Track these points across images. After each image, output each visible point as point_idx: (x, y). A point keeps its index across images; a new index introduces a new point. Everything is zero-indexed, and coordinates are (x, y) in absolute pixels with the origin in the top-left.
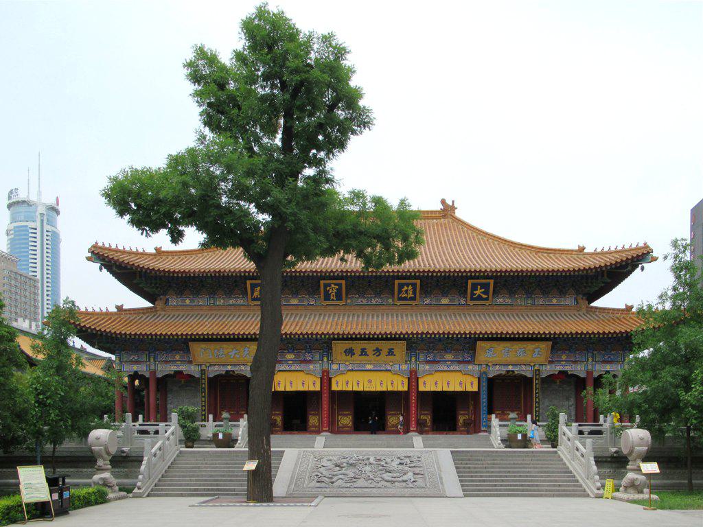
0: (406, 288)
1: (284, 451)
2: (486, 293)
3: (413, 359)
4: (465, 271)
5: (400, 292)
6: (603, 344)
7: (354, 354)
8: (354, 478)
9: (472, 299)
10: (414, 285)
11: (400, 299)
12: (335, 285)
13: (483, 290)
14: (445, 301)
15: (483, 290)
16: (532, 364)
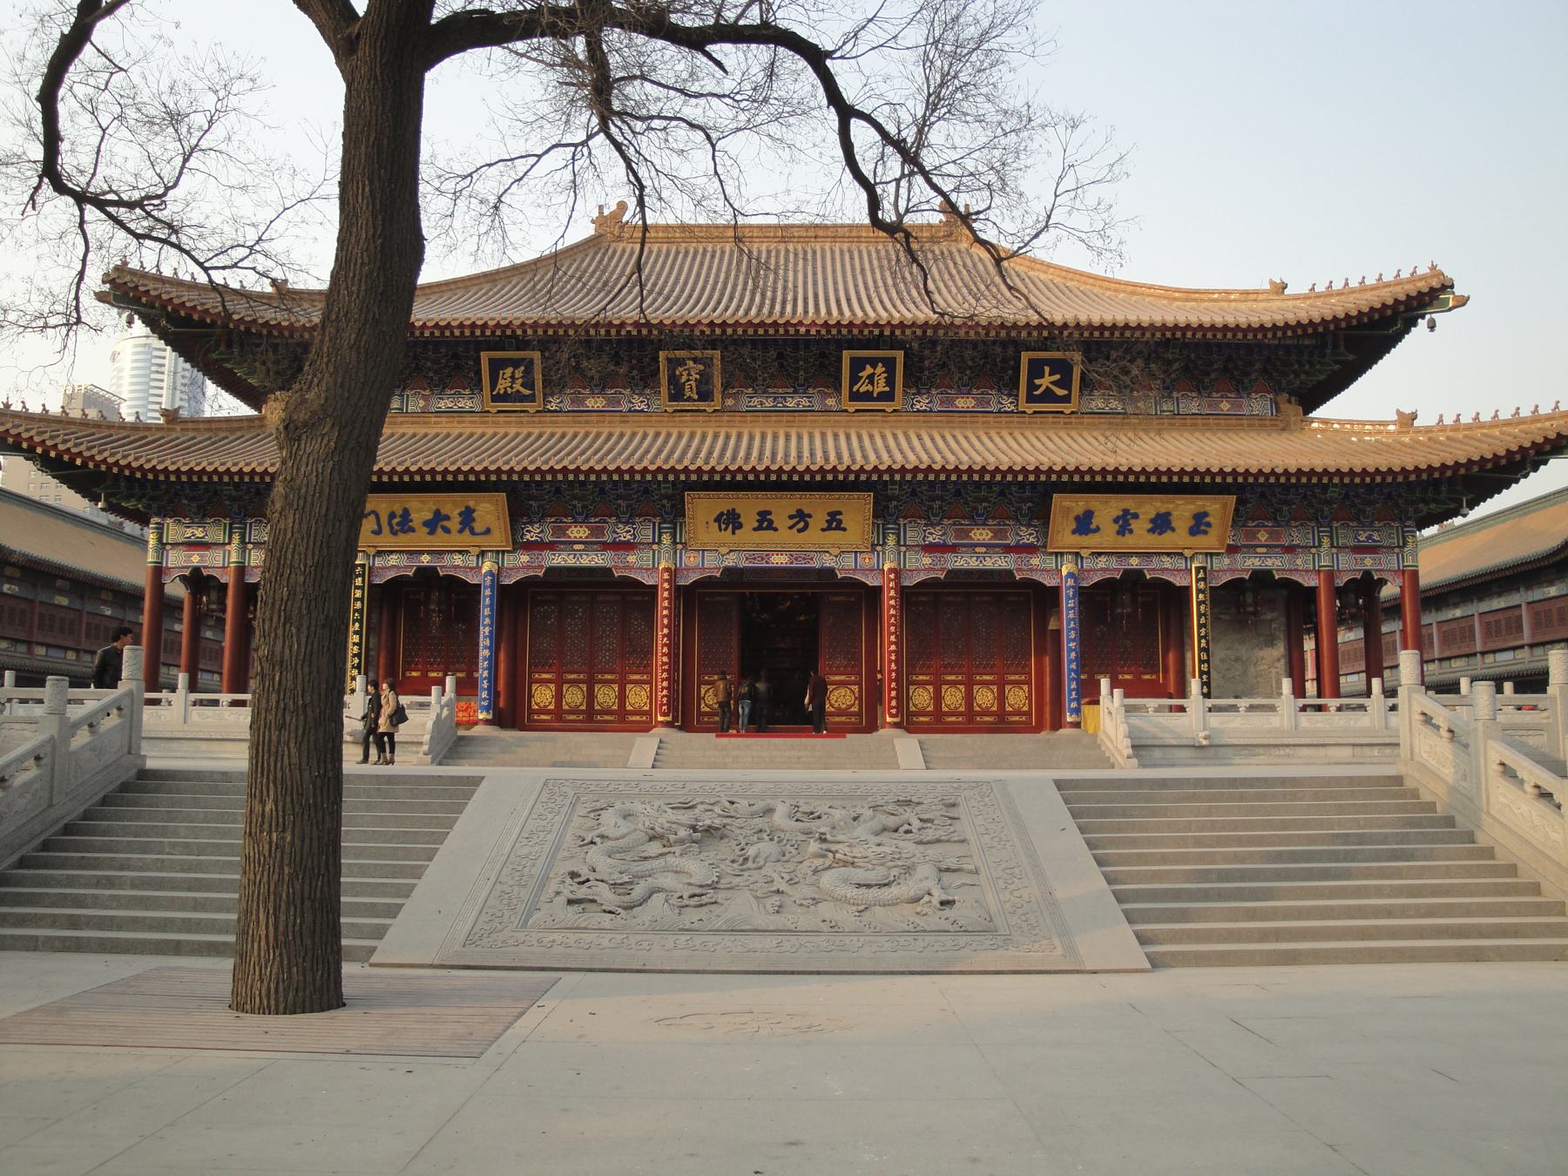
0: (869, 370)
1: (476, 781)
2: (1065, 383)
3: (891, 540)
4: (943, 468)
5: (854, 379)
6: (1353, 505)
7: (740, 526)
8: (713, 886)
9: (1031, 399)
10: (890, 365)
11: (855, 397)
12: (695, 360)
13: (1057, 377)
14: (963, 403)
15: (1057, 377)
16: (1187, 553)
